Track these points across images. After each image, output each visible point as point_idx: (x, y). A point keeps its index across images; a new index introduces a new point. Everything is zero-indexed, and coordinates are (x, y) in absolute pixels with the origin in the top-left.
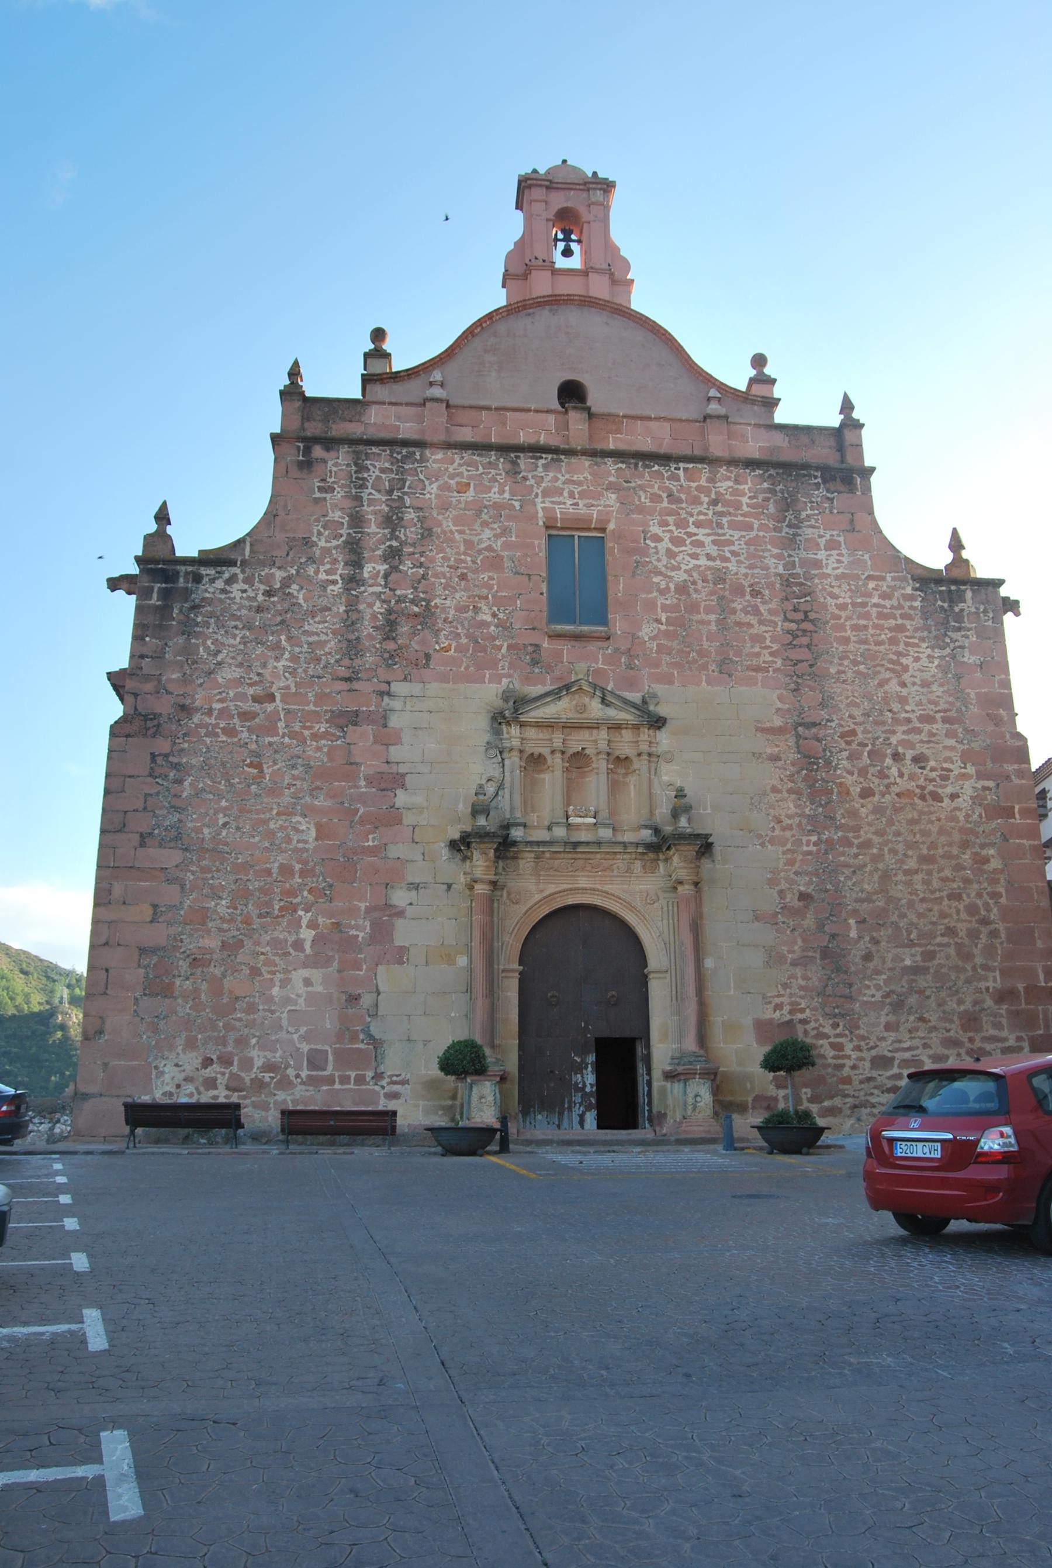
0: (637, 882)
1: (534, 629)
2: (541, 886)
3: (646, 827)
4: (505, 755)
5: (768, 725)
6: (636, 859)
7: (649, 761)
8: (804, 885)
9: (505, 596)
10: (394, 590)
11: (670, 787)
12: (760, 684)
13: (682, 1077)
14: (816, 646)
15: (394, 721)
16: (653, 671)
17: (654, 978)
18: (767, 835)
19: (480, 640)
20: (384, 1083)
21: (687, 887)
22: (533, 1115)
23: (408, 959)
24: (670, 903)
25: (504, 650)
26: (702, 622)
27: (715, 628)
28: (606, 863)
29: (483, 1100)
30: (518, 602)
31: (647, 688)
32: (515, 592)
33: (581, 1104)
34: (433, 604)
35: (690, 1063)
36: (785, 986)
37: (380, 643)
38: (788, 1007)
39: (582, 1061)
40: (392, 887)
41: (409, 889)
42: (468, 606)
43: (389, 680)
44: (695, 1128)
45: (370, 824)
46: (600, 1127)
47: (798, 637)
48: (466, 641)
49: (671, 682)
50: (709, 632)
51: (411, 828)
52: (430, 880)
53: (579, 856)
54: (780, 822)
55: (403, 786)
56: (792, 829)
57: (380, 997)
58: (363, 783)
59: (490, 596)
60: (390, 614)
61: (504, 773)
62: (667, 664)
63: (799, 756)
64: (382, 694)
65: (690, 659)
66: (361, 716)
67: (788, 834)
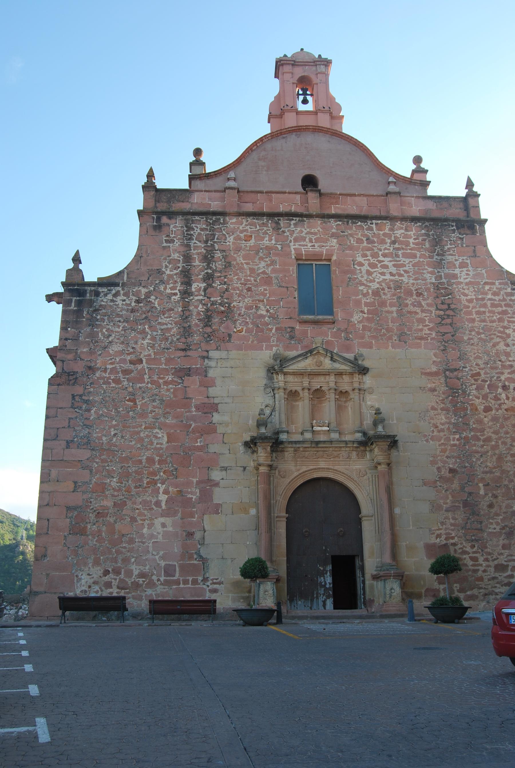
0: (354, 464)
1: (290, 318)
2: (298, 467)
3: (359, 432)
4: (276, 392)
5: (428, 371)
6: (353, 450)
7: (359, 393)
8: (452, 464)
9: (274, 300)
10: (210, 298)
11: (372, 408)
12: (423, 347)
13: (383, 578)
14: (455, 324)
15: (211, 373)
18: (429, 435)
19: (260, 326)
20: (208, 583)
21: (383, 466)
22: (296, 602)
24: (374, 476)
25: (274, 331)
26: (388, 312)
27: (396, 315)
28: (335, 453)
29: (267, 593)
30: (281, 303)
31: (357, 351)
32: (279, 297)
33: (324, 594)
34: (232, 305)
35: (388, 570)
36: (442, 523)
37: (202, 328)
38: (444, 535)
40: (212, 469)
41: (221, 470)
42: (253, 306)
43: (208, 350)
44: (391, 608)
47: (444, 319)
48: (251, 326)
49: (371, 347)
50: (392, 317)
53: (320, 449)
54: (437, 427)
55: (217, 411)
56: (444, 431)
57: (205, 533)
60: (208, 312)
61: (275, 402)
62: (369, 336)
63: (447, 388)
64: (204, 358)
67: (442, 434)
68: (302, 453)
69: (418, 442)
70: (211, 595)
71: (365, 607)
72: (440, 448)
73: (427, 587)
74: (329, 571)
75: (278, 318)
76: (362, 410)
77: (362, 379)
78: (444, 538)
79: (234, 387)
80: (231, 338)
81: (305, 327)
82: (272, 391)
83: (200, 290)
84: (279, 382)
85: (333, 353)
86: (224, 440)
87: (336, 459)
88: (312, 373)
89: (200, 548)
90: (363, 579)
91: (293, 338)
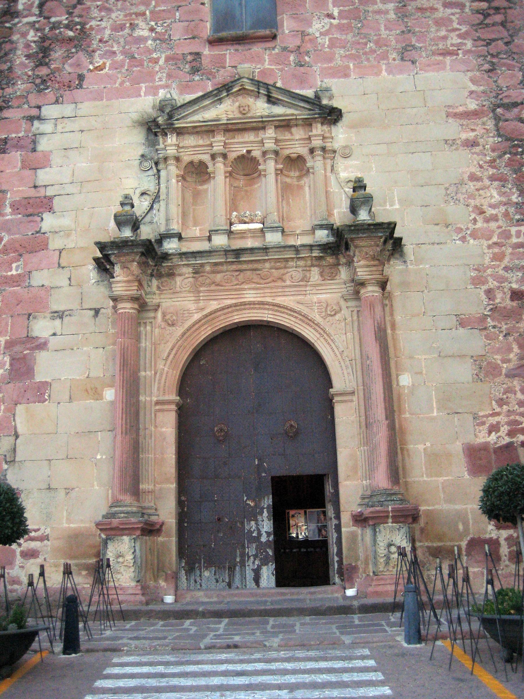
1: (194, 38)
2: (202, 304)
3: (321, 227)
4: (161, 166)
5: (461, 109)
6: (313, 266)
7: (324, 158)
8: (517, 282)
9: (164, 11)
10: (48, 18)
12: (448, 67)
14: (512, 22)
15: (43, 145)
16: (325, 65)
17: (338, 402)
18: (468, 229)
19: (136, 56)
21: (370, 288)
22: (198, 573)
23: (49, 396)
25: (161, 62)
26: (379, 12)
27: (394, 16)
29: (121, 560)
30: (177, 14)
31: (319, 83)
32: (174, 5)
33: (255, 556)
34: (88, 26)
36: (501, 402)
37: (33, 70)
38: (506, 426)
39: (256, 505)
40: (35, 318)
41: (53, 318)
42: (125, 25)
43: (40, 104)
45: (14, 252)
46: (280, 583)
47: (489, 15)
48: (122, 57)
49: (346, 75)
50: (388, 20)
51: (57, 253)
52: (75, 306)
53: (245, 266)
54: (482, 212)
55: (50, 209)
56: (497, 220)
57: (18, 441)
58: (8, 210)
59: (148, 13)
60: (44, 42)
62: (341, 56)
63: (500, 140)
64: (31, 119)
65: (367, 50)
66: (10, 143)
67: (493, 225)
68: (209, 275)
69: (446, 243)
70: (25, 561)
71: (342, 580)
72: (491, 251)
73: (471, 536)
74: (267, 508)
75: (171, 40)
76: (329, 189)
77: (330, 132)
78: (506, 432)
79: (85, 165)
80: (83, 81)
81: (217, 51)
82: (154, 166)
83: (33, 7)
84: (167, 148)
85: (270, 87)
86: (61, 261)
87: (279, 283)
88: (230, 127)
89: (6, 470)
90: (336, 522)
91: (198, 71)
